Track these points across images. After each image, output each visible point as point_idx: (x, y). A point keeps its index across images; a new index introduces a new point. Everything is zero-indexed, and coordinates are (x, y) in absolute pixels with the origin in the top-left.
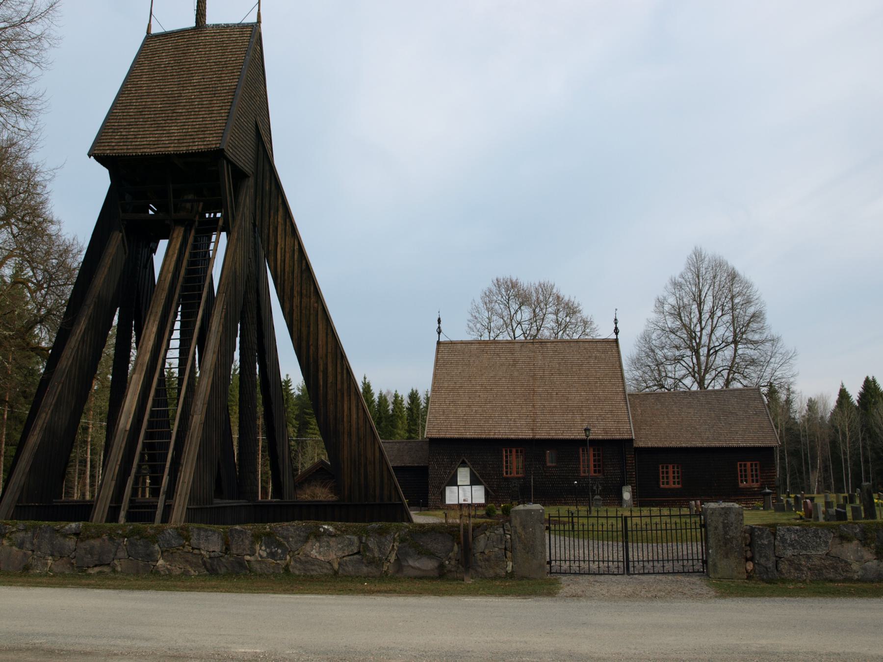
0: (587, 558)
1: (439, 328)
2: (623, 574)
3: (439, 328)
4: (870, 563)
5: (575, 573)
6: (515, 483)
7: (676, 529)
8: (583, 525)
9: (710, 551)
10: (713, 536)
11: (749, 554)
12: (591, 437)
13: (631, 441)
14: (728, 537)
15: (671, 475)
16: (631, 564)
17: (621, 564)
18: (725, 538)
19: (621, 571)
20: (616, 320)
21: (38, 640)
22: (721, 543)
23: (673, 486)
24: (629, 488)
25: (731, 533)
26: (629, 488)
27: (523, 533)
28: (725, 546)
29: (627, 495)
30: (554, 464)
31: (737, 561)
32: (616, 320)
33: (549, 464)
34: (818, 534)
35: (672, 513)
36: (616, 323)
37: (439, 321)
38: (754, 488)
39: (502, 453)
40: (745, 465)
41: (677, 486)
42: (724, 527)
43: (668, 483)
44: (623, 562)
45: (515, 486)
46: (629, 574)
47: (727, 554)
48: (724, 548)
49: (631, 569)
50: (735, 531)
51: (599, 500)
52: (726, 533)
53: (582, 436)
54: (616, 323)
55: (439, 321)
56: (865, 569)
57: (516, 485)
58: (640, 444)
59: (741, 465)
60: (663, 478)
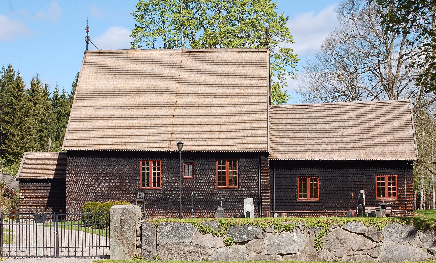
1: (87, 36)
2: (53, 257)
3: (87, 36)
4: (221, 249)
6: (140, 195)
10: (113, 229)
11: (139, 243)
12: (184, 149)
13: (266, 154)
14: (124, 230)
16: (60, 250)
17: (52, 250)
19: (52, 254)
23: (311, 199)
30: (191, 177)
33: (186, 176)
34: (186, 227)
37: (87, 30)
39: (139, 165)
40: (383, 179)
41: (315, 199)
42: (121, 223)
44: (54, 248)
46: (57, 256)
49: (60, 254)
50: (129, 225)
51: (222, 212)
53: (175, 148)
55: (87, 30)
56: (217, 253)
57: (141, 197)
58: (275, 156)
59: (379, 179)
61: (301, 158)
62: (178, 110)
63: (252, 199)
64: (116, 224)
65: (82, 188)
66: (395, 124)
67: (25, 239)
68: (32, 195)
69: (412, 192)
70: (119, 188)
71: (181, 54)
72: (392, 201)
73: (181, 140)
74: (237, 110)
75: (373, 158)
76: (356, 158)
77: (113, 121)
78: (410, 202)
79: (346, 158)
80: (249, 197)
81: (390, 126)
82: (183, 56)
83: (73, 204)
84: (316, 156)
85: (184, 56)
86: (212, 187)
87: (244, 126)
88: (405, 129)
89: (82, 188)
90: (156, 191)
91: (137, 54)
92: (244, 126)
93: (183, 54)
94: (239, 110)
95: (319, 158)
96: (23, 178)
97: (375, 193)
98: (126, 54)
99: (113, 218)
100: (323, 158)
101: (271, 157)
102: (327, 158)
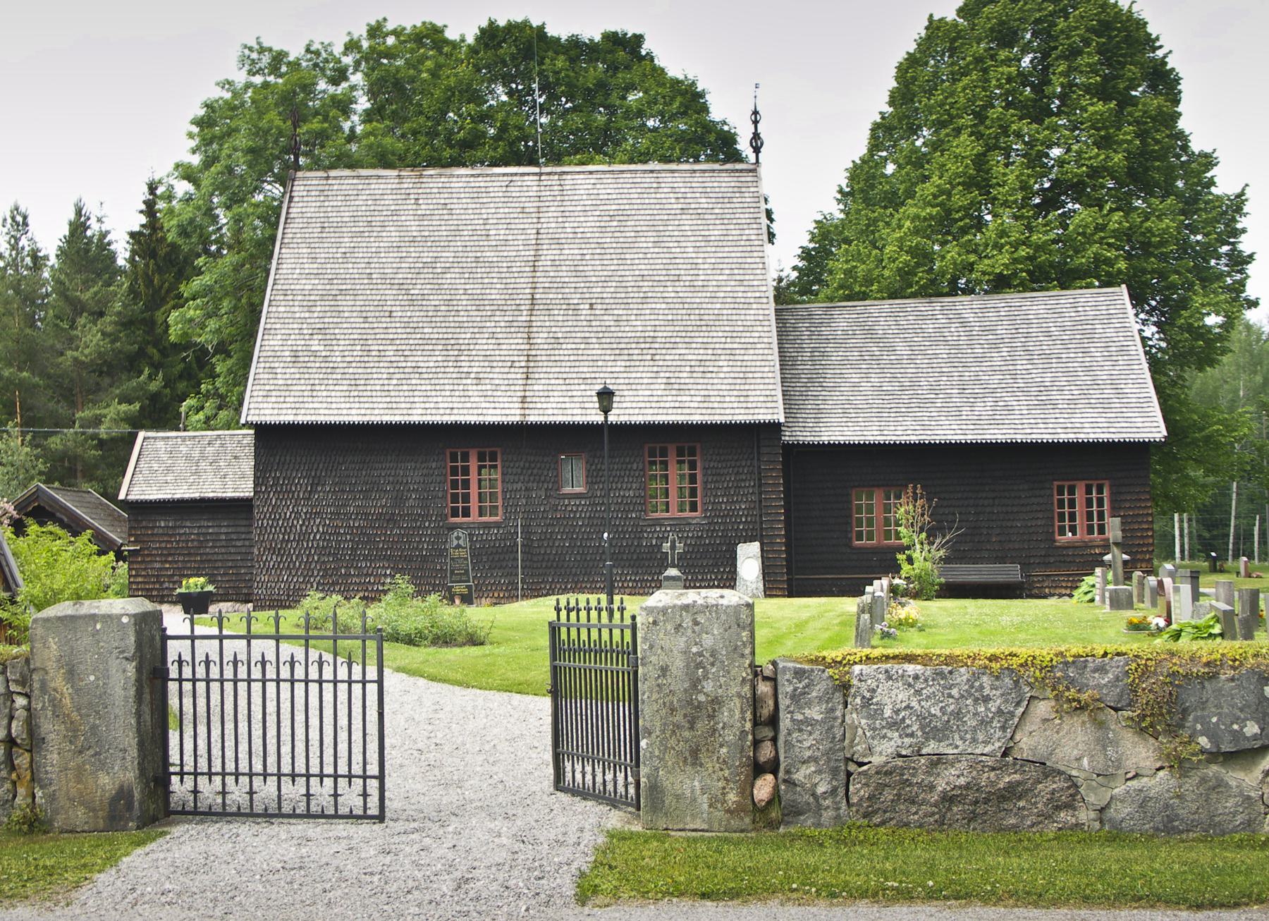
0: (329, 770)
5: (351, 816)
6: (458, 538)
7: (292, 682)
8: (263, 663)
9: (643, 743)
10: (655, 696)
14: (702, 698)
15: (673, 493)
18: (690, 703)
20: (756, 113)
21: (986, 743)
22: (678, 718)
24: (755, 547)
25: (709, 686)
26: (755, 547)
27: (66, 690)
28: (692, 728)
29: (749, 560)
31: (726, 773)
32: (756, 113)
34: (982, 687)
35: (199, 630)
36: (756, 122)
38: (1095, 547)
43: (466, 513)
45: (458, 546)
47: (695, 752)
48: (687, 734)
52: (695, 684)
54: (756, 122)
57: (461, 542)
60: (493, 496)
61: (863, 438)
62: (537, 318)
63: (757, 544)
64: (664, 676)
65: (295, 522)
66: (1093, 350)
67: (272, 752)
68: (161, 542)
69: (1147, 522)
70: (391, 519)
71: (537, 178)
72: (1098, 546)
73: (608, 381)
74: (692, 317)
75: (1048, 436)
76: (1004, 437)
77: (372, 348)
78: (1145, 549)
79: (979, 437)
80: (751, 539)
81: (1080, 355)
82: (541, 183)
83: (272, 563)
84: (900, 433)
85: (545, 183)
86: (634, 516)
87: (713, 358)
88: (1121, 363)
89: (295, 522)
90: (487, 526)
91: (425, 180)
92: (713, 358)
93: (543, 178)
94: (697, 317)
95: (908, 438)
96: (137, 497)
97: (1053, 525)
98: (397, 181)
99: (651, 647)
100: (920, 437)
101: (787, 437)
102: (929, 438)
